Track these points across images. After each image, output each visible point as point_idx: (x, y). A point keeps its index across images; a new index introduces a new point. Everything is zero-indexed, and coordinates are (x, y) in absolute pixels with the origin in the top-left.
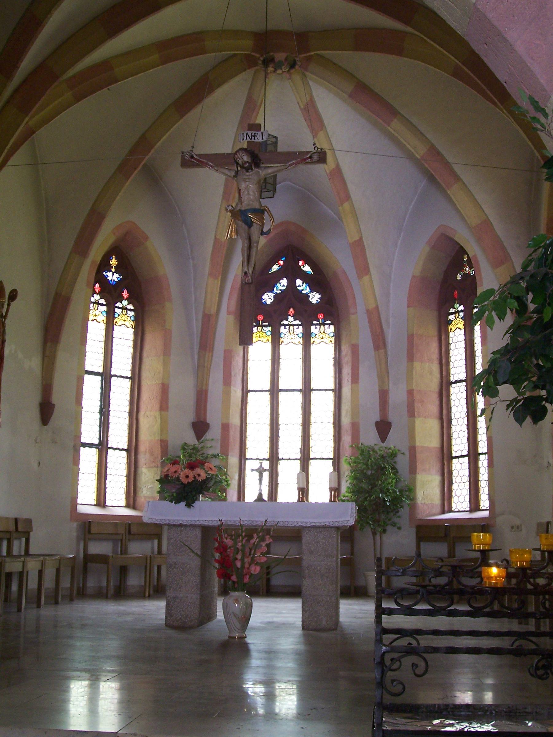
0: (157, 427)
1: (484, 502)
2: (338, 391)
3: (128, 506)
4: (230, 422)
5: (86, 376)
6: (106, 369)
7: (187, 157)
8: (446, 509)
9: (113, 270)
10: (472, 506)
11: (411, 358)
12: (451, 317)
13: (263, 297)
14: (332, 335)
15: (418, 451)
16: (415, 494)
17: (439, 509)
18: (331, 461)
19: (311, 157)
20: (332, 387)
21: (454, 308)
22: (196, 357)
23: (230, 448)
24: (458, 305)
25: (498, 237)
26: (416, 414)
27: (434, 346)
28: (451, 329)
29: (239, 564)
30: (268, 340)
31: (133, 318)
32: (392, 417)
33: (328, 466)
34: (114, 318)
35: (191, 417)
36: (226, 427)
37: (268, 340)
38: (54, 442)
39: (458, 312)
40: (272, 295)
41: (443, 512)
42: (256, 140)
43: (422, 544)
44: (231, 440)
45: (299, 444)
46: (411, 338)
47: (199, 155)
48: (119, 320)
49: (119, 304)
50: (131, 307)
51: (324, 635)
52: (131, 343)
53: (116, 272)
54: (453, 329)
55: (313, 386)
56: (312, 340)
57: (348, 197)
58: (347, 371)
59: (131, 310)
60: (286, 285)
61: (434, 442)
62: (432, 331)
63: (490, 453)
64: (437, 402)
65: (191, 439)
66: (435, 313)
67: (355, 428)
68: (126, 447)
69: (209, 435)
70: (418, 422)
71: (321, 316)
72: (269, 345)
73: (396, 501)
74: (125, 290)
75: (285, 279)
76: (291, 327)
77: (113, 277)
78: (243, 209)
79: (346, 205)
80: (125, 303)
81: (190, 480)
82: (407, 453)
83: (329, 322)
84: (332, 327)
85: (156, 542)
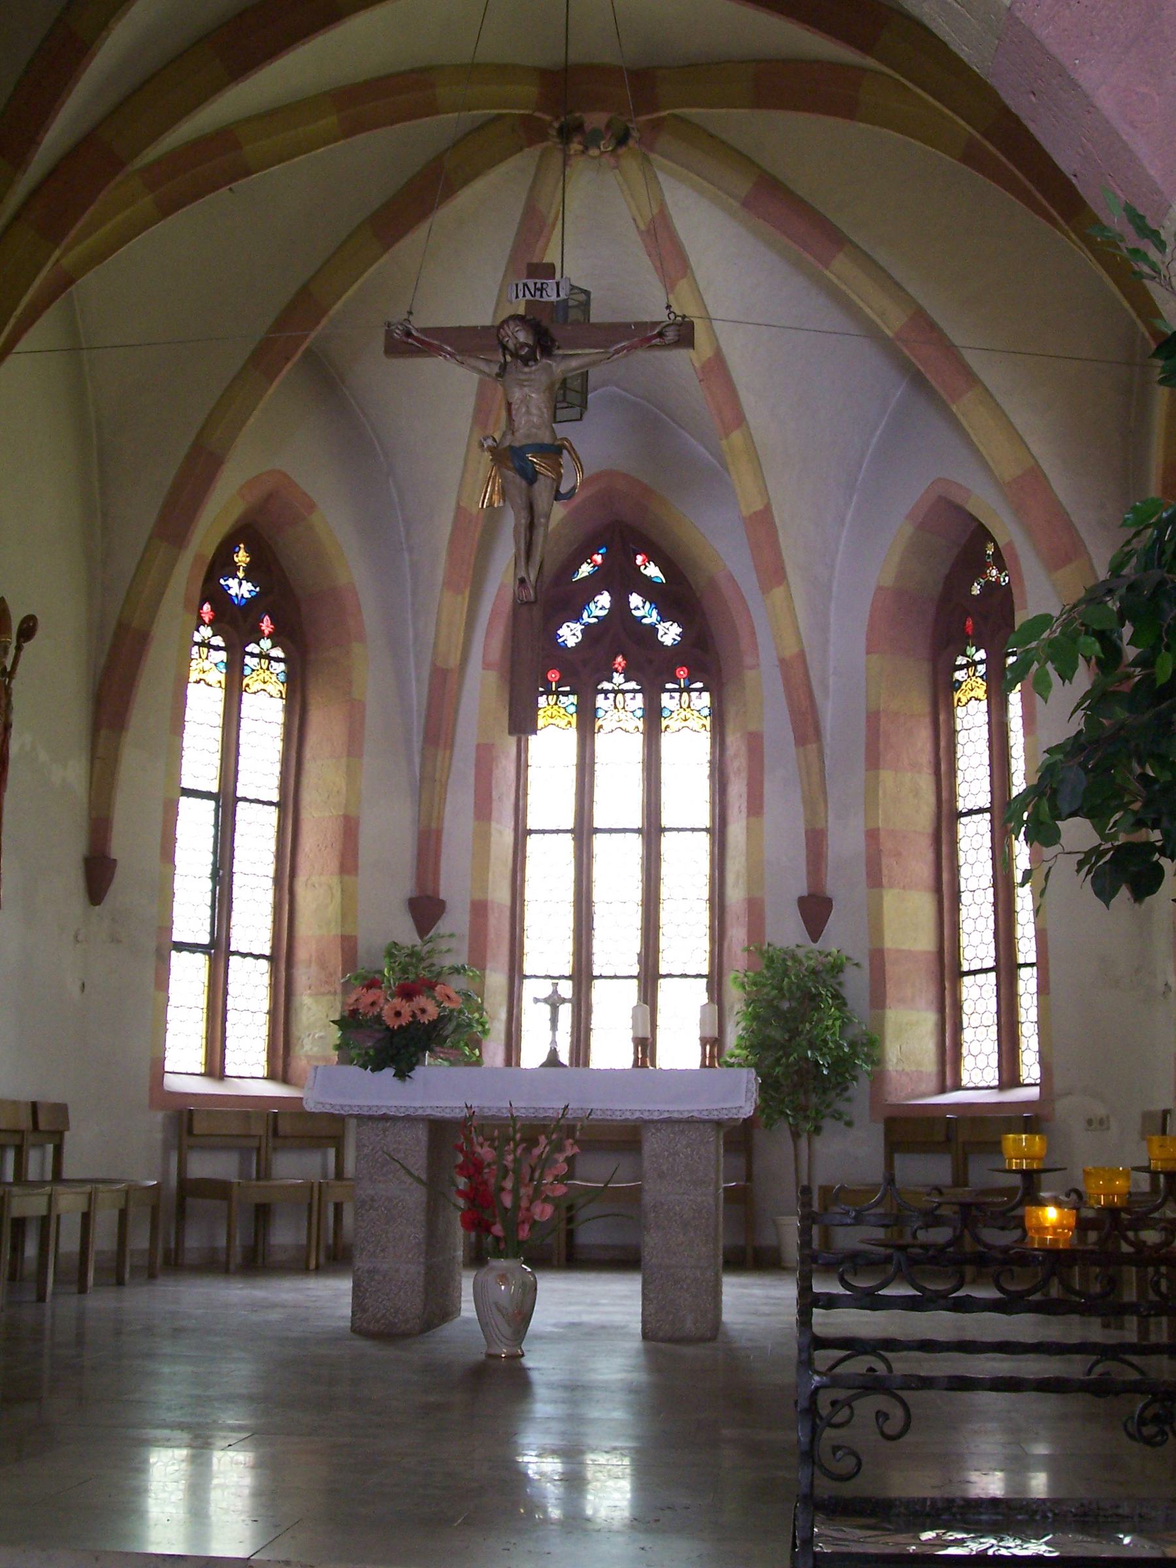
0: (333, 909)
1: (1030, 1068)
2: (718, 832)
3: (271, 1076)
4: (489, 899)
6: (225, 785)
7: (398, 334)
8: (949, 1082)
9: (241, 574)
10: (1005, 1077)
11: (873, 761)
12: (959, 675)
13: (560, 632)
14: (706, 712)
15: (889, 959)
16: (883, 1051)
17: (933, 1083)
18: (705, 980)
20: (707, 823)
21: (965, 655)
22: (417, 760)
23: (489, 954)
24: (974, 649)
25: (1059, 503)
26: (885, 880)
27: (923, 737)
28: (959, 700)
29: (507, 1201)
30: (569, 723)
31: (282, 677)
32: (833, 887)
33: (698, 992)
34: (243, 676)
35: (405, 887)
36: (480, 909)
37: (569, 723)
38: (115, 940)
39: (975, 664)
40: (578, 628)
41: (943, 1090)
42: (545, 299)
43: (898, 1158)
44: (492, 936)
45: (635, 944)
46: (873, 719)
47: (423, 331)
48: (252, 681)
49: (252, 648)
50: (278, 653)
51: (688, 1351)
52: (278, 731)
53: (247, 578)
54: (964, 700)
55: (665, 822)
56: (664, 723)
57: (740, 420)
58: (737, 790)
59: (278, 660)
60: (608, 605)
61: (924, 941)
62: (920, 704)
63: (1042, 964)
64: (929, 856)
65: (405, 933)
66: (926, 667)
67: (755, 910)
68: (267, 951)
69: (444, 926)
70: (889, 898)
71: (682, 673)
72: (572, 735)
73: (843, 1067)
74: (267, 618)
75: (606, 594)
76: (620, 696)
77: (240, 589)
78: (517, 444)
79: (736, 437)
80: (266, 644)
81: (404, 1021)
82: (866, 964)
83: (699, 685)
84: (706, 696)
85: (332, 1152)
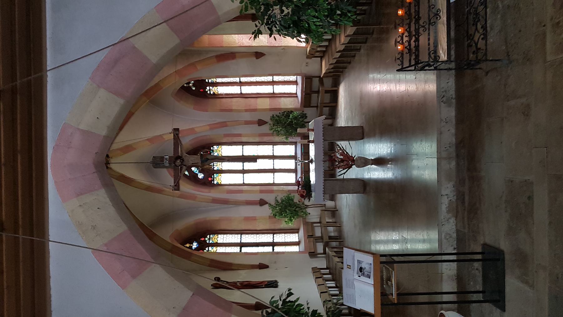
1: (293, 78)
4: (259, 190)
5: (242, 251)
6: (238, 245)
7: (176, 188)
8: (295, 96)
9: (191, 245)
10: (295, 84)
11: (231, 110)
12: (212, 93)
13: (200, 178)
14: (218, 147)
17: (295, 99)
18: (274, 146)
19: (177, 134)
20: (241, 146)
21: (207, 91)
23: (271, 189)
24: (206, 89)
25: (183, 68)
27: (224, 100)
28: (217, 93)
30: (220, 175)
31: (213, 235)
32: (256, 119)
34: (214, 243)
35: (258, 208)
36: (261, 192)
37: (220, 175)
38: (275, 262)
39: (210, 89)
40: (199, 174)
42: (168, 158)
44: (266, 189)
45: (267, 161)
47: (174, 183)
48: (215, 241)
49: (208, 242)
50: (208, 236)
52: (225, 236)
53: (192, 244)
54: (217, 92)
56: (220, 155)
57: (161, 136)
58: (236, 139)
59: (210, 236)
60: (194, 168)
61: (267, 100)
62: (218, 100)
63: (272, 75)
66: (210, 100)
67: (261, 135)
68: (272, 235)
70: (259, 107)
72: (223, 175)
74: (201, 239)
75: (192, 168)
76: (214, 165)
77: (195, 245)
78: (201, 162)
79: (165, 137)
80: (206, 239)
83: (212, 148)
84: (214, 147)
85: (315, 225)
